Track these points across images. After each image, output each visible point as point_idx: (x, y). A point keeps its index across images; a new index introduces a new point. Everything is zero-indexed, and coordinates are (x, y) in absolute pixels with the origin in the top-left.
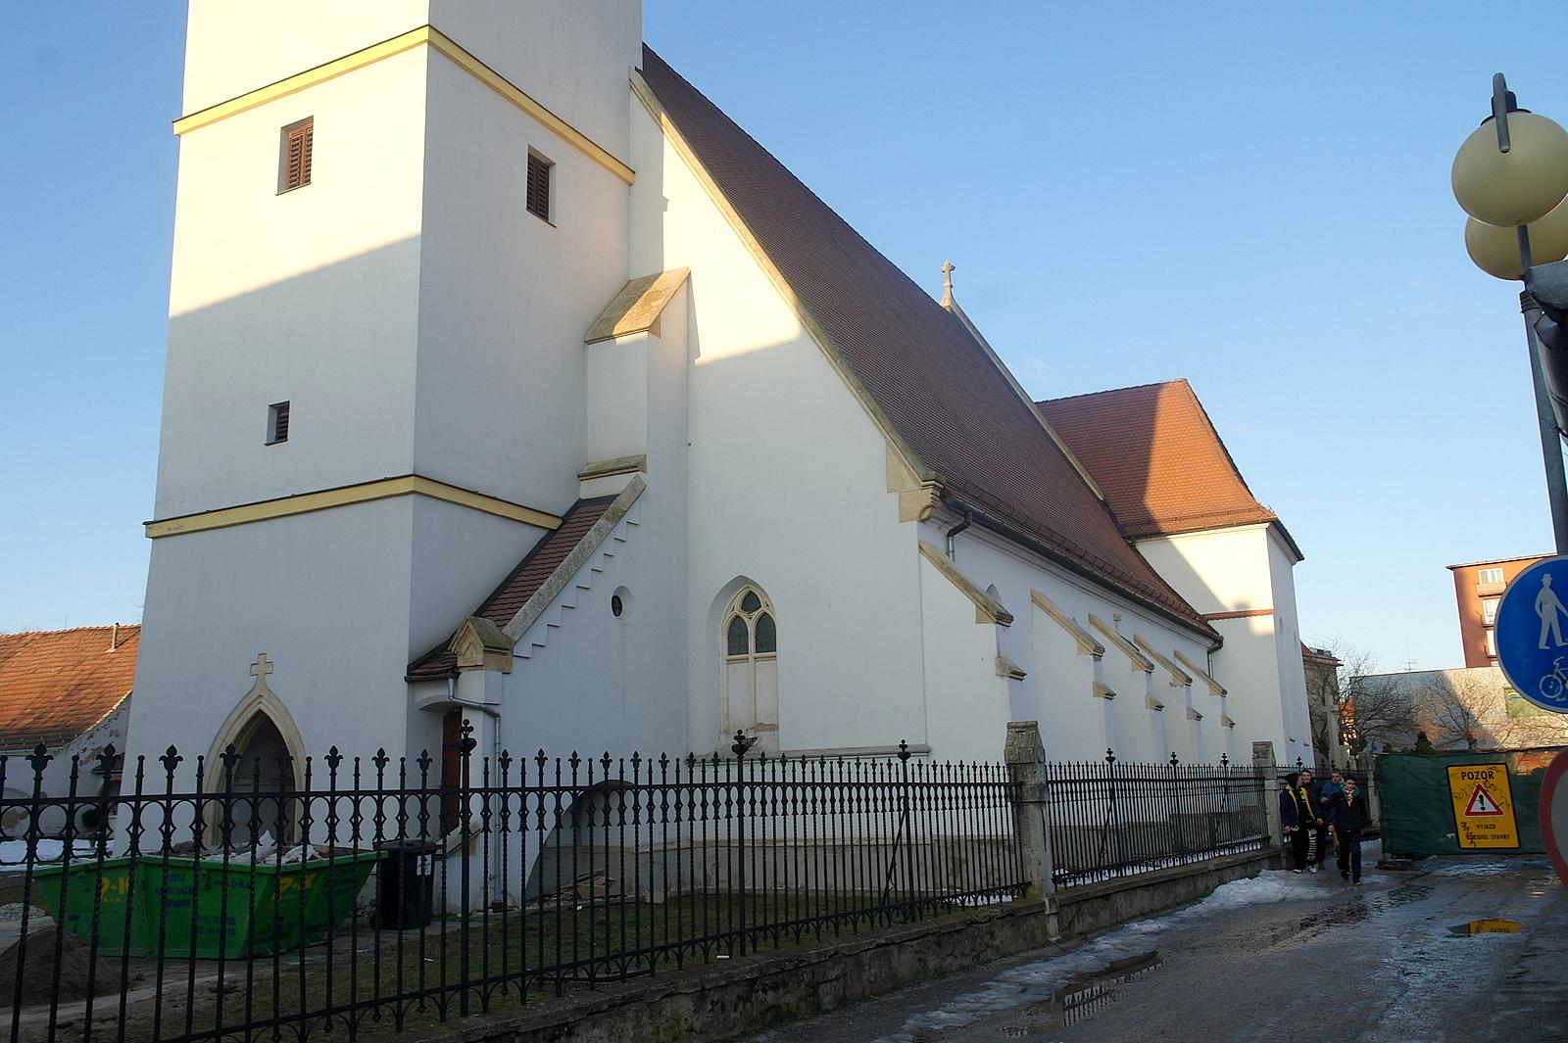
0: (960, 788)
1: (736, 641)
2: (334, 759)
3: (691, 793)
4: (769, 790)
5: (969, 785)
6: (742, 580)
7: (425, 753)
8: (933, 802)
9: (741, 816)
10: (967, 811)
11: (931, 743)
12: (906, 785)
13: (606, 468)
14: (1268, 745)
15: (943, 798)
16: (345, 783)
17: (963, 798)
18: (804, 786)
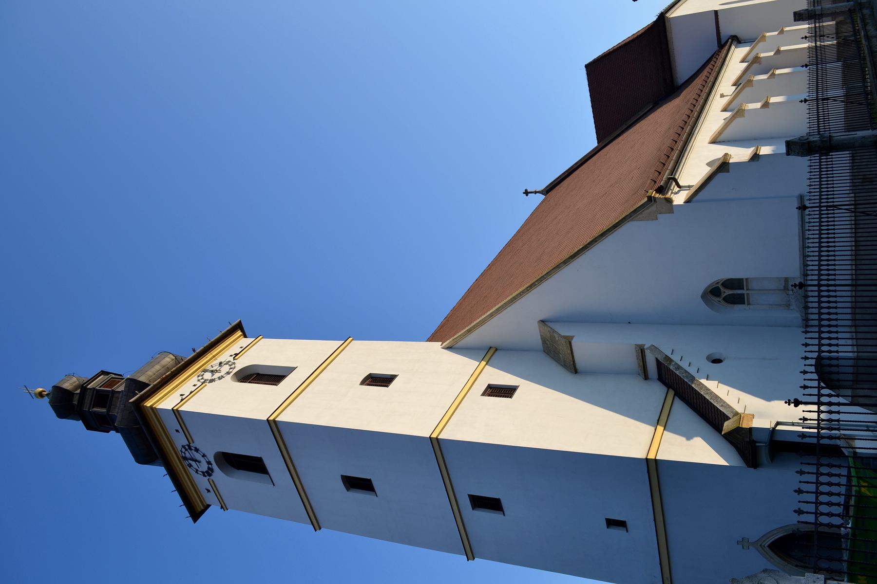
0: (822, 180)
1: (738, 300)
2: (800, 512)
3: (823, 345)
4: (822, 263)
5: (820, 165)
6: (704, 296)
7: (797, 472)
8: (830, 258)
9: (835, 285)
10: (837, 240)
11: (797, 193)
12: (820, 207)
13: (641, 364)
14: (795, 13)
15: (828, 260)
16: (812, 508)
17: (828, 247)
18: (820, 260)
